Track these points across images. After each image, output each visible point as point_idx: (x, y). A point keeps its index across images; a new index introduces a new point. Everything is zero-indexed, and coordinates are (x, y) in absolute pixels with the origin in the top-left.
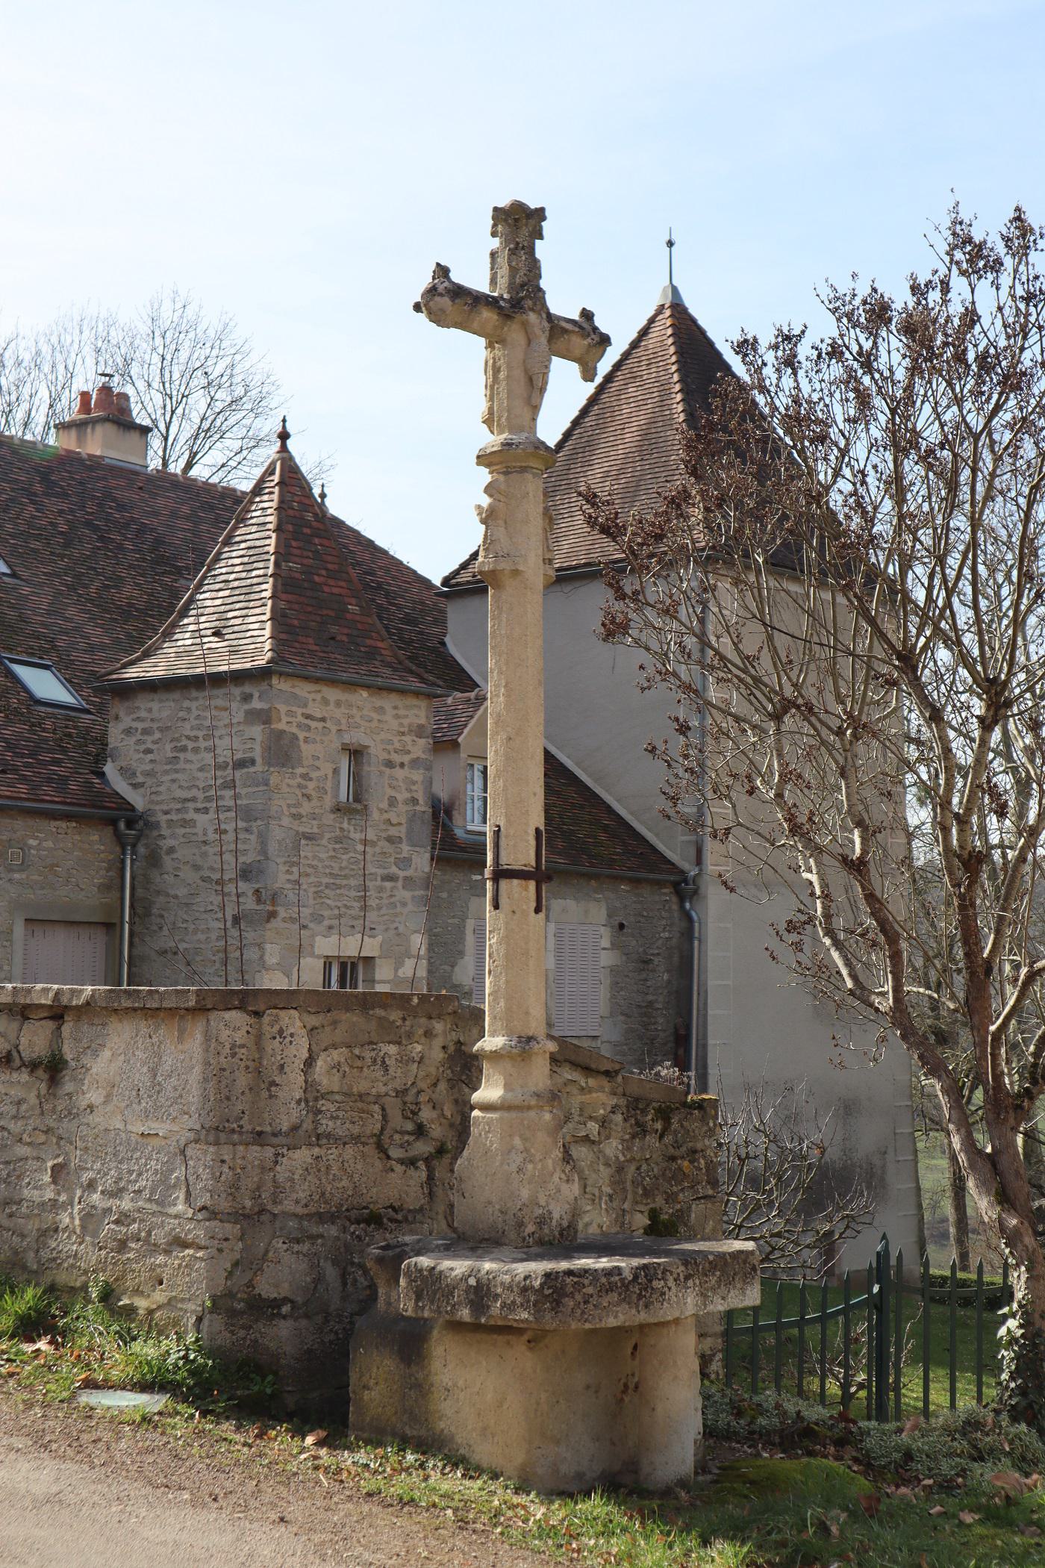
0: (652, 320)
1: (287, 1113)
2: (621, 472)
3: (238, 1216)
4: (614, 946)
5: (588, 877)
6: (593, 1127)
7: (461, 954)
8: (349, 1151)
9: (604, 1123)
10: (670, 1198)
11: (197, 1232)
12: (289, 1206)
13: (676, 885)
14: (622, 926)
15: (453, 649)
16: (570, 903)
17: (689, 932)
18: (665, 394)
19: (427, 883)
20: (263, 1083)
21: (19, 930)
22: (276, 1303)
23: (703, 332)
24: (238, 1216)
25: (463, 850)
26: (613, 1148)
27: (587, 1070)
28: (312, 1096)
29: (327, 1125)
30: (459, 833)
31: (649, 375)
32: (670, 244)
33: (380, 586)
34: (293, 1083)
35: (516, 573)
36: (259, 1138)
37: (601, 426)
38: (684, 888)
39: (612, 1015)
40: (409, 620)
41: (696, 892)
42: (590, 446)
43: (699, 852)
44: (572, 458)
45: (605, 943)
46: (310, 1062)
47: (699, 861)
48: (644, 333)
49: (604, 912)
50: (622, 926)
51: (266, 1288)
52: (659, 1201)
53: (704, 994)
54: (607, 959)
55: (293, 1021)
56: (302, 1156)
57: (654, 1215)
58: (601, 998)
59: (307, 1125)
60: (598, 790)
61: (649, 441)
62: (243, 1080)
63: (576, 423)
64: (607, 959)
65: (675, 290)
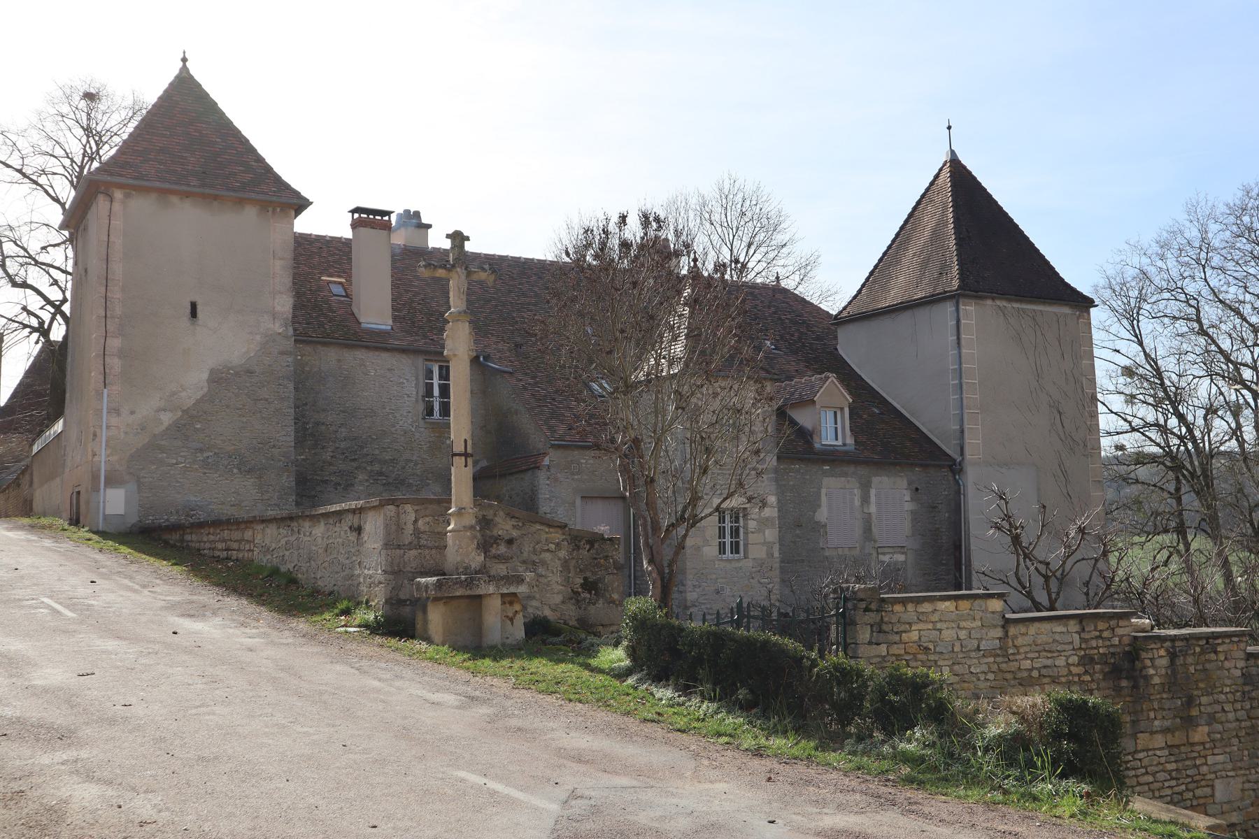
0: (941, 170)
1: (407, 537)
2: (922, 252)
3: (393, 573)
4: (912, 500)
5: (895, 464)
6: (553, 546)
7: (819, 506)
8: (434, 551)
9: (558, 545)
10: (594, 573)
11: (382, 579)
12: (408, 569)
13: (950, 467)
14: (917, 489)
15: (841, 352)
16: (885, 479)
17: (958, 493)
18: (945, 209)
19: (776, 471)
20: (400, 529)
21: (578, 502)
22: (405, 601)
23: (970, 173)
24: (393, 573)
25: (815, 454)
26: (563, 554)
27: (550, 526)
28: (417, 533)
29: (423, 542)
30: (817, 446)
31: (938, 199)
32: (949, 128)
33: (804, 322)
34: (409, 528)
35: (455, 355)
36: (399, 547)
37: (914, 229)
38: (955, 468)
39: (913, 535)
40: (818, 338)
41: (961, 470)
42: (908, 239)
43: (962, 449)
44: (899, 248)
45: (907, 498)
46: (416, 521)
47: (962, 453)
48: (937, 176)
49: (905, 482)
50: (917, 489)
51: (402, 597)
52: (588, 574)
53: (967, 522)
54: (909, 506)
55: (408, 508)
56: (414, 552)
57: (585, 579)
58: (906, 526)
59: (415, 542)
60: (912, 420)
61: (937, 235)
62: (394, 528)
63: (902, 228)
64: (909, 506)
65: (953, 152)
